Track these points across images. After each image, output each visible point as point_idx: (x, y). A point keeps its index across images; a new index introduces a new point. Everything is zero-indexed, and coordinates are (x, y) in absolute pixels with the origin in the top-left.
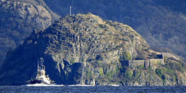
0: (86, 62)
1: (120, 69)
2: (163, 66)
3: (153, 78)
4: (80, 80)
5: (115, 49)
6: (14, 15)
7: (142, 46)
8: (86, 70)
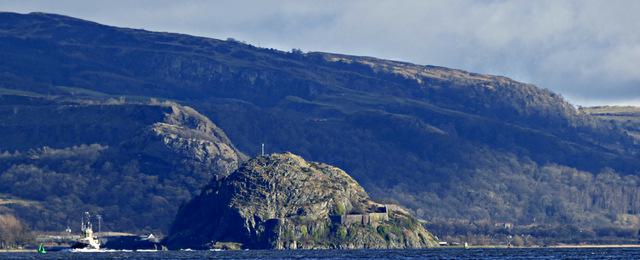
2: (386, 221)
5: (323, 200)
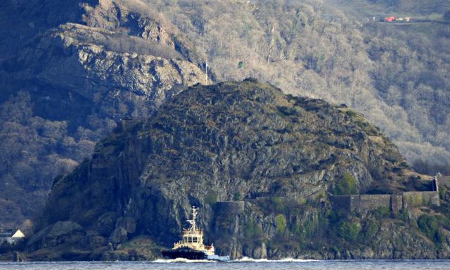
0: (244, 200)
1: (330, 217)
2: (435, 208)
3: (412, 239)
4: (229, 245)
5: (317, 168)
6: (123, 85)
7: (387, 159)
8: (245, 220)
